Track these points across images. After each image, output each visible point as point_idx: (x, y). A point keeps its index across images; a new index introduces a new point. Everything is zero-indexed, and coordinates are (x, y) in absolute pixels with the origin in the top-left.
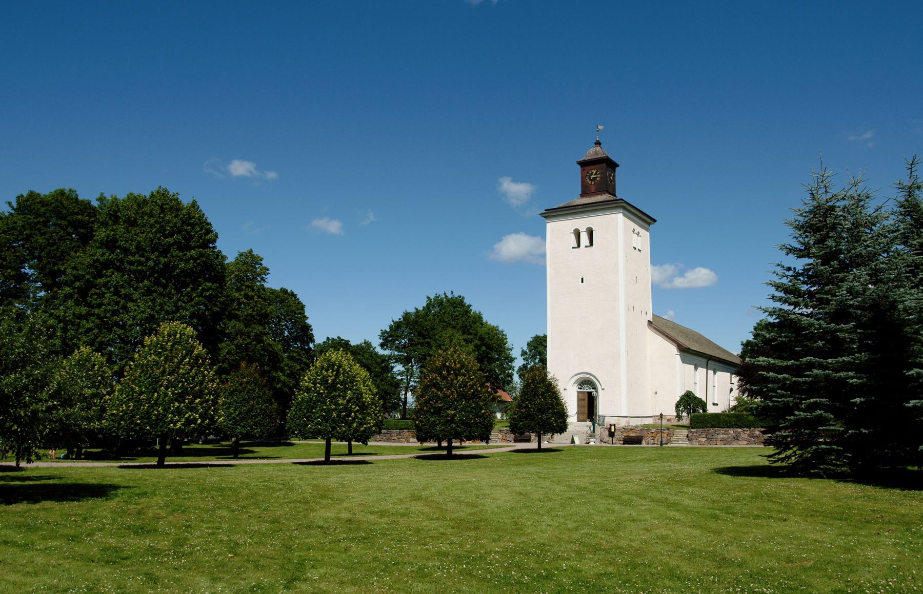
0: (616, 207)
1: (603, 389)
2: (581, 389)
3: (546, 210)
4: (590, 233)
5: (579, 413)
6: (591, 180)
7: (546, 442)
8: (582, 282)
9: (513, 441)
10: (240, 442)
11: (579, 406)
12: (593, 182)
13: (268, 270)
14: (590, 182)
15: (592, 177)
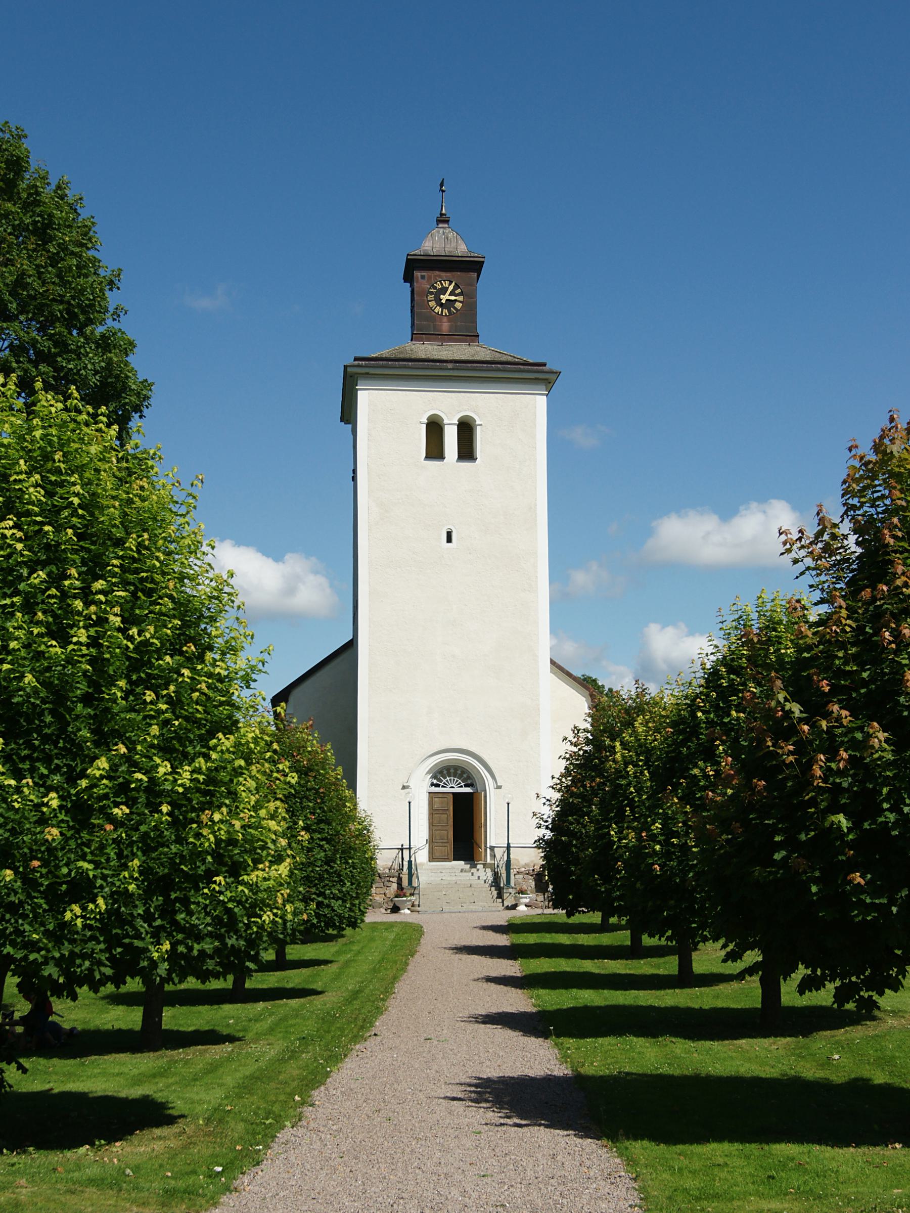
0: (536, 379)
1: (499, 787)
2: (437, 786)
3: (356, 359)
4: (466, 429)
5: (431, 841)
6: (441, 305)
7: (407, 911)
8: (449, 540)
9: (552, 907)
10: (248, 964)
11: (432, 825)
12: (445, 311)
13: (875, 442)
14: (438, 309)
15: (444, 298)
